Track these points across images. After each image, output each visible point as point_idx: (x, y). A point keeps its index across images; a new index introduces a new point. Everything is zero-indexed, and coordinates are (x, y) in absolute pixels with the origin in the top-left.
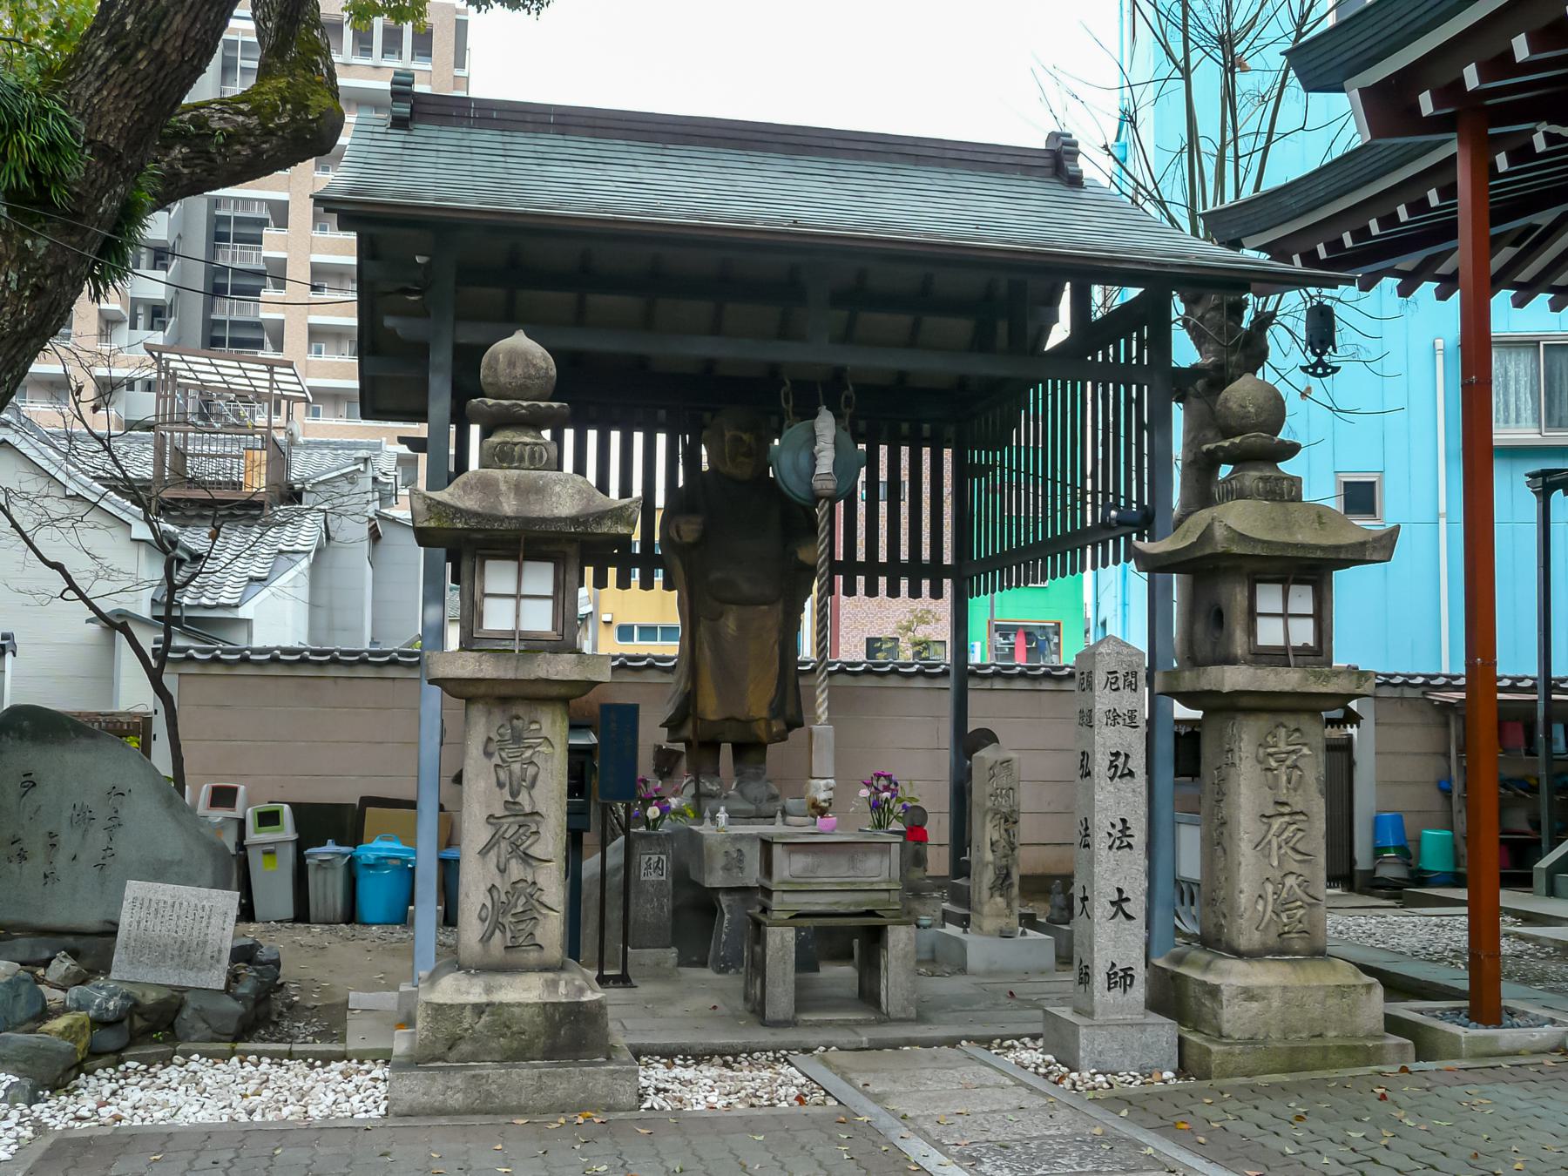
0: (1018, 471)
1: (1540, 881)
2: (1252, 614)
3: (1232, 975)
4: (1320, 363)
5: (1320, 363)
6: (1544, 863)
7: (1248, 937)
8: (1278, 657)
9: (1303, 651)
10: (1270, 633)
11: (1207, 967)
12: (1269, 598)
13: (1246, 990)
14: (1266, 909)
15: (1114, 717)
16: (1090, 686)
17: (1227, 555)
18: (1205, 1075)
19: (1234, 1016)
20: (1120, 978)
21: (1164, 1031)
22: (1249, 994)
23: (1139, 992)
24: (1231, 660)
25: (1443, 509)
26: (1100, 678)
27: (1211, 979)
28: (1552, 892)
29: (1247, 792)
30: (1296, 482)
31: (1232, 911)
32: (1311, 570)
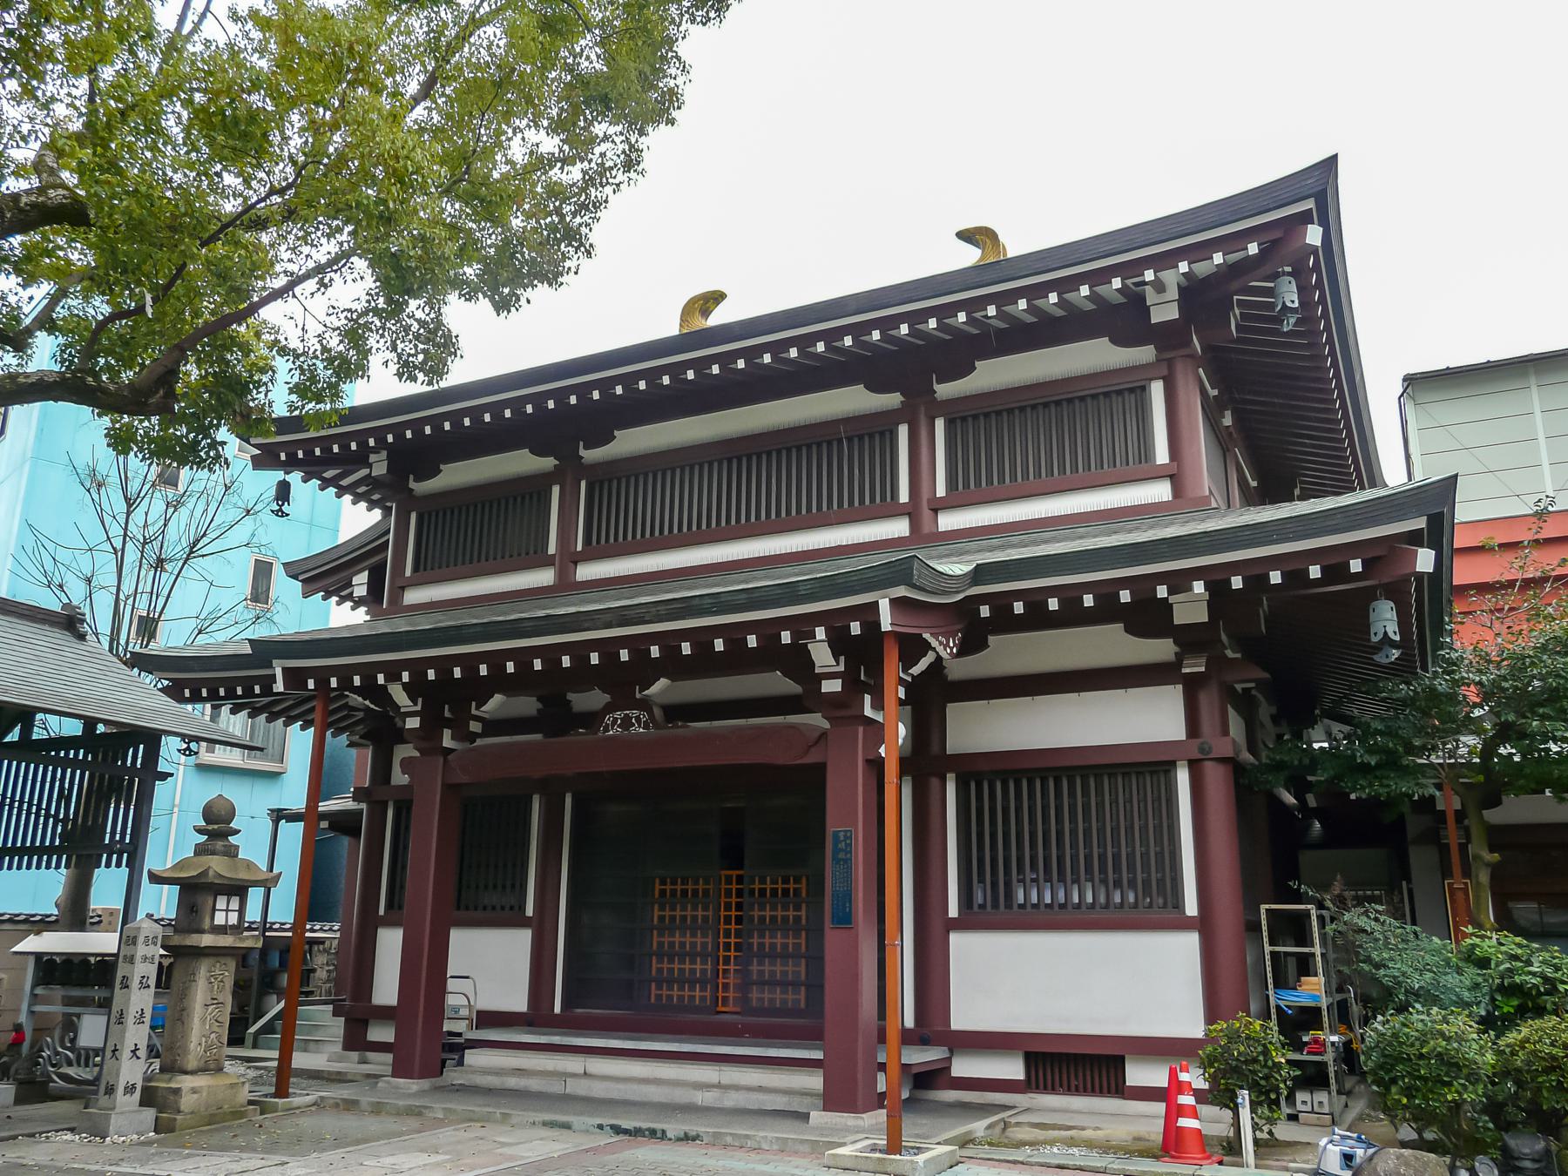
0: (21, 802)
1: (249, 1040)
2: (214, 910)
3: (186, 1082)
4: (188, 748)
5: (188, 748)
6: (252, 1030)
7: (192, 1063)
8: (223, 930)
9: (232, 927)
10: (220, 919)
11: (170, 1080)
12: (221, 902)
13: (193, 1089)
14: (200, 1050)
15: (145, 959)
16: (134, 943)
17: (212, 884)
18: (172, 1130)
19: (187, 1102)
20: (130, 1089)
21: (150, 1114)
22: (194, 1091)
23: (137, 1095)
24: (202, 932)
25: (177, 801)
26: (141, 939)
27: (173, 1085)
28: (255, 1046)
29: (200, 993)
30: (237, 847)
31: (186, 1051)
32: (238, 890)
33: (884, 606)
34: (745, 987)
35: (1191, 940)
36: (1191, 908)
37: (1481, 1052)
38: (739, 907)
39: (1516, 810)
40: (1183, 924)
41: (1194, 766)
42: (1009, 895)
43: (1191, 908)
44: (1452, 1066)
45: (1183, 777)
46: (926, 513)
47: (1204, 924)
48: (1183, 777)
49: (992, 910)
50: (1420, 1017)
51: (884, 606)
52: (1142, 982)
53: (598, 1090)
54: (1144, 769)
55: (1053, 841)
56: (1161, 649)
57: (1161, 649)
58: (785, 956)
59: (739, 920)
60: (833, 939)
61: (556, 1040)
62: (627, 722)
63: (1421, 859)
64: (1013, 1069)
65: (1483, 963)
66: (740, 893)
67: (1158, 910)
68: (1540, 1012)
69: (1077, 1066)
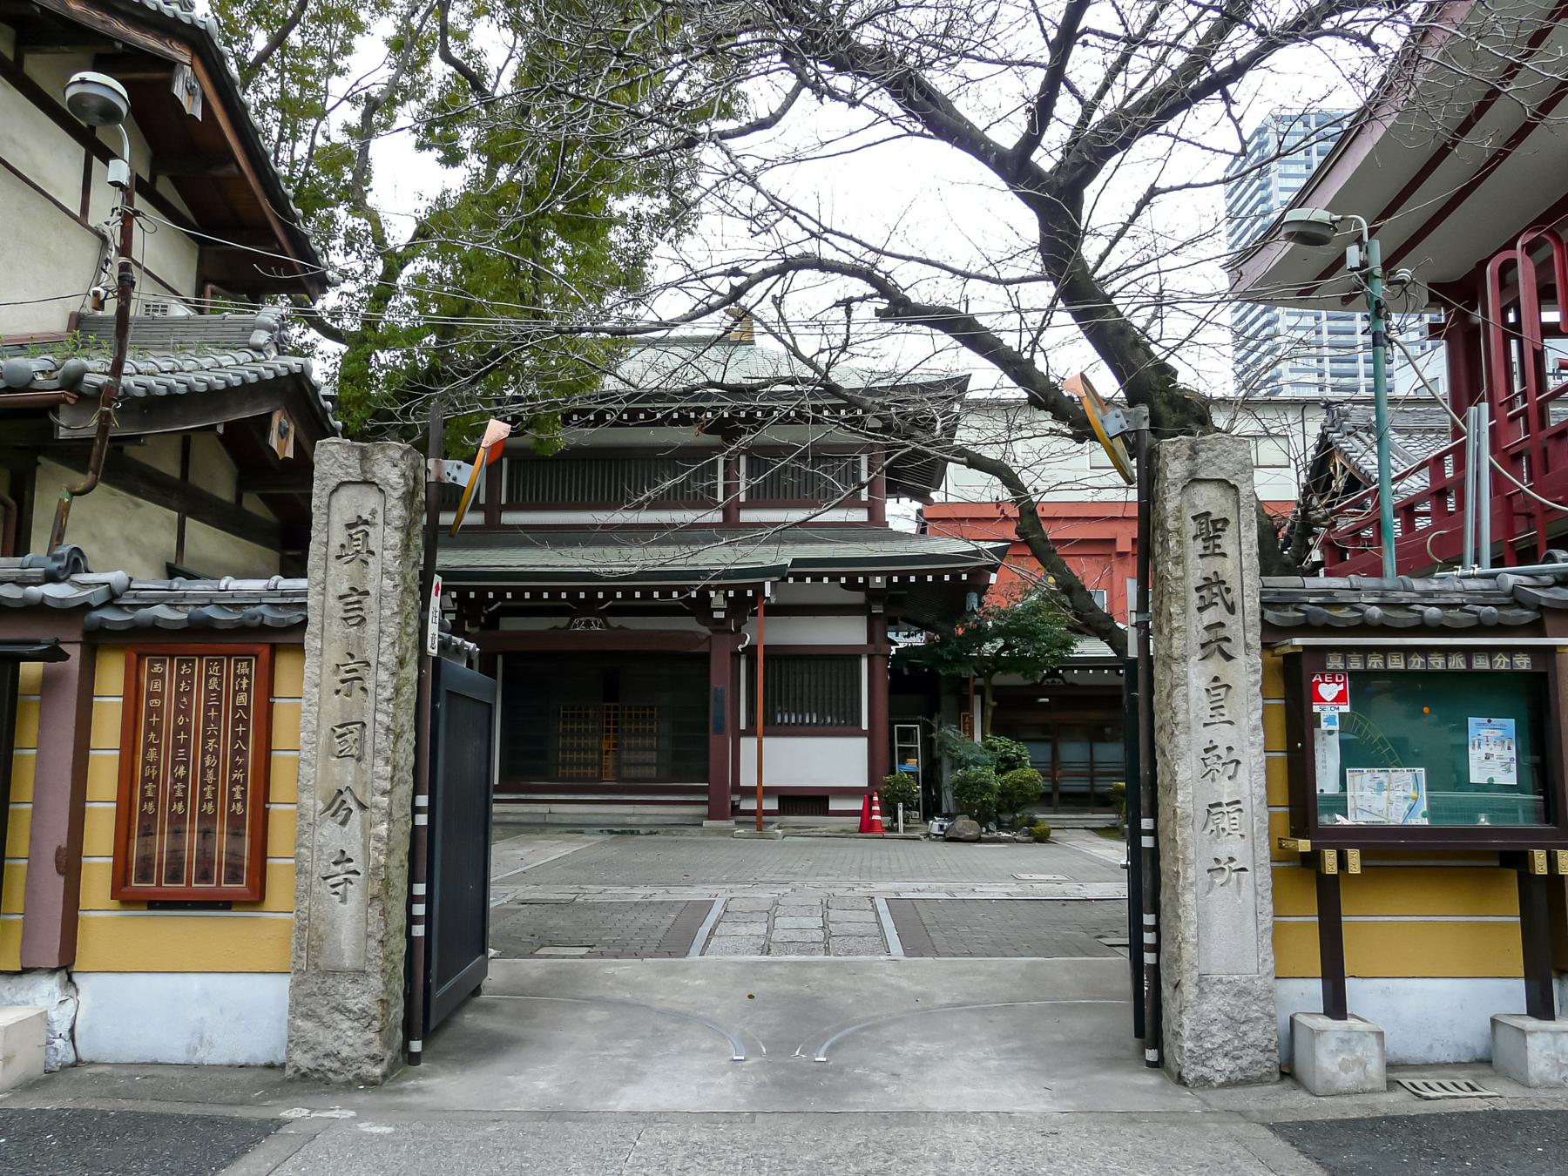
33: (768, 585)
34: (618, 766)
35: (865, 740)
36: (865, 726)
37: (996, 781)
38: (615, 723)
39: (999, 679)
40: (860, 734)
41: (870, 658)
42: (775, 718)
43: (865, 726)
44: (986, 787)
45: (864, 662)
46: (734, 510)
47: (871, 734)
48: (864, 662)
49: (775, 729)
50: (974, 770)
51: (768, 585)
52: (839, 761)
53: (556, 819)
54: (845, 659)
55: (805, 692)
56: (858, 597)
57: (858, 597)
58: (644, 749)
59: (615, 731)
60: (714, 739)
61: (523, 796)
62: (588, 624)
63: (947, 702)
64: (771, 804)
65: (995, 749)
66: (616, 716)
67: (849, 727)
68: (1015, 768)
69: (806, 802)
